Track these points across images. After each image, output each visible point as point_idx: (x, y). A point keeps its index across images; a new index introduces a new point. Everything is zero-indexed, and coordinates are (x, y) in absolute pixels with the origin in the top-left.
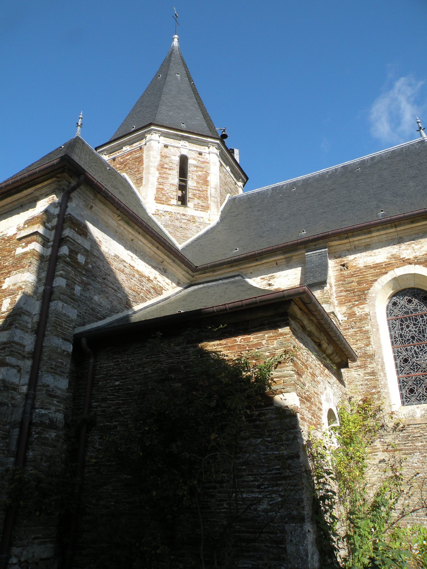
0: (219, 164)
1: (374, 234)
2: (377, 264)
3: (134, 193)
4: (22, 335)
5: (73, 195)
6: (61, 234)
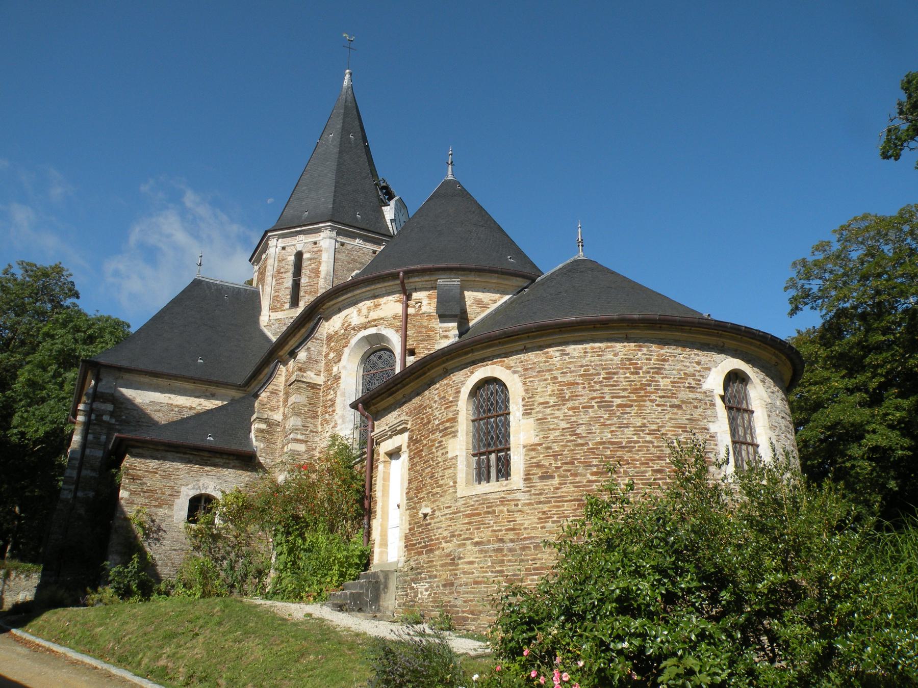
5: (101, 377)
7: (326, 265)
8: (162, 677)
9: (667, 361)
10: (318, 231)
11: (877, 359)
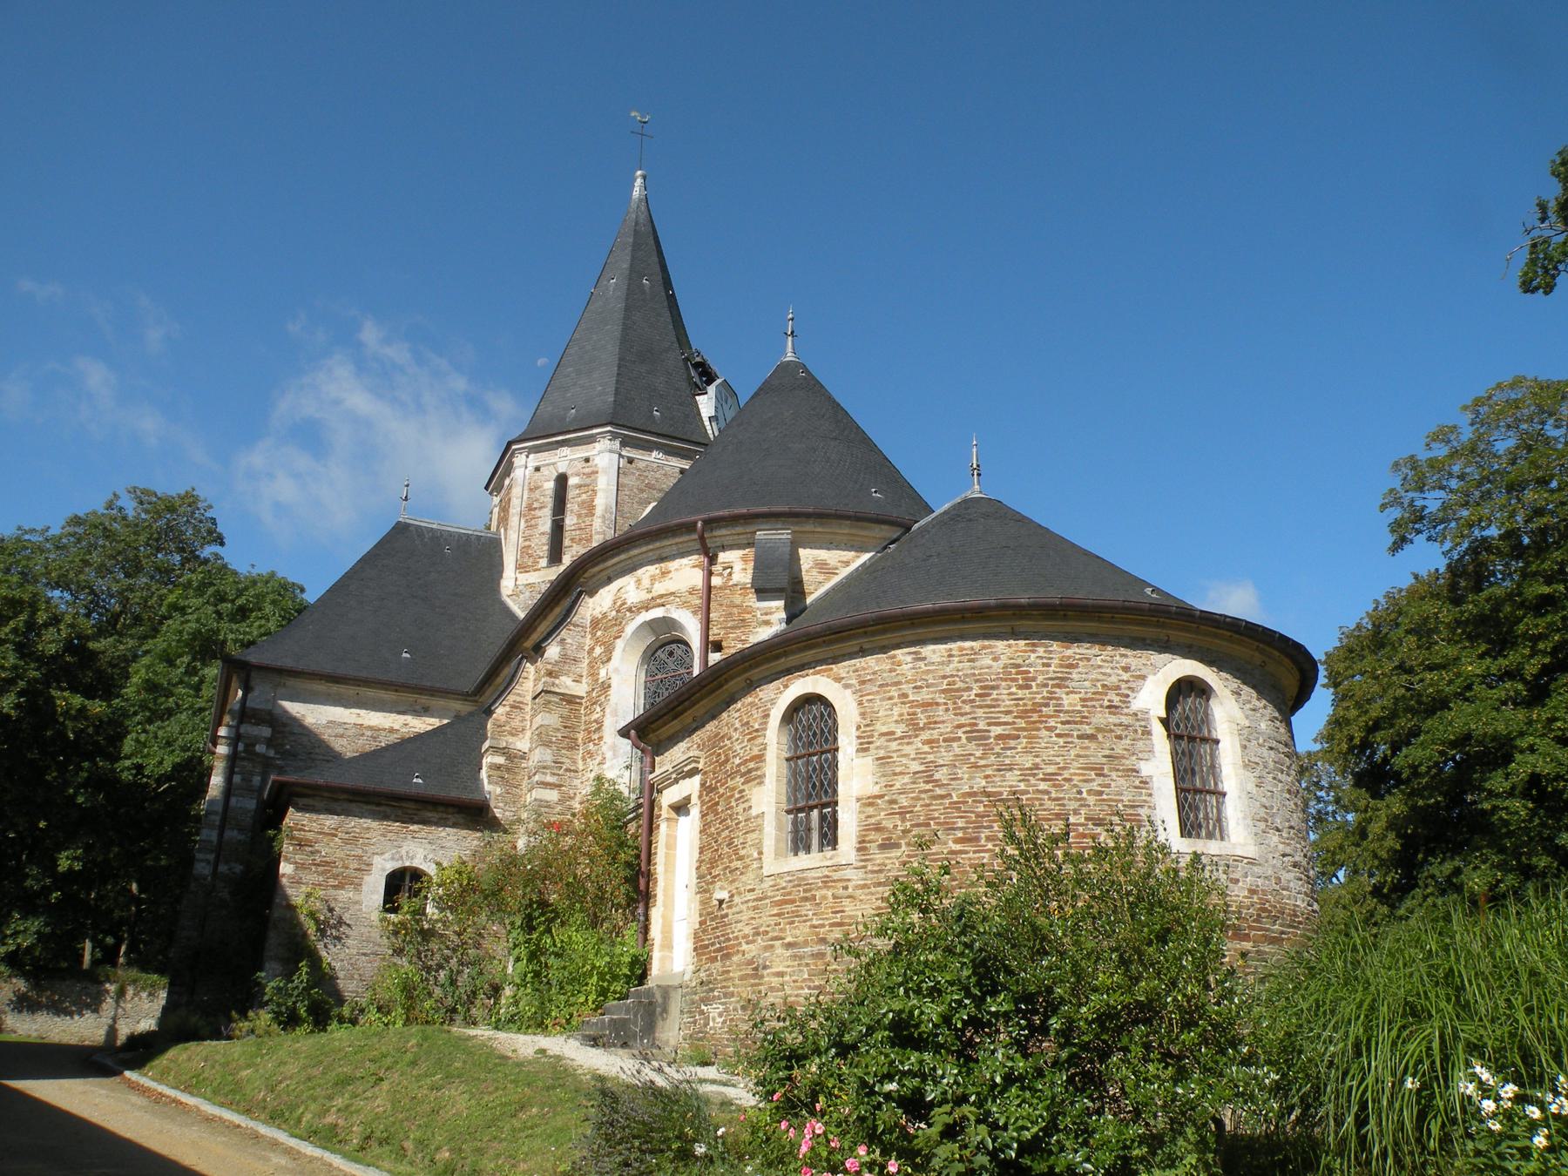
5: (252, 683)
7: (604, 498)
8: (330, 1140)
9: (1077, 666)
10: (591, 440)
11: (1537, 626)
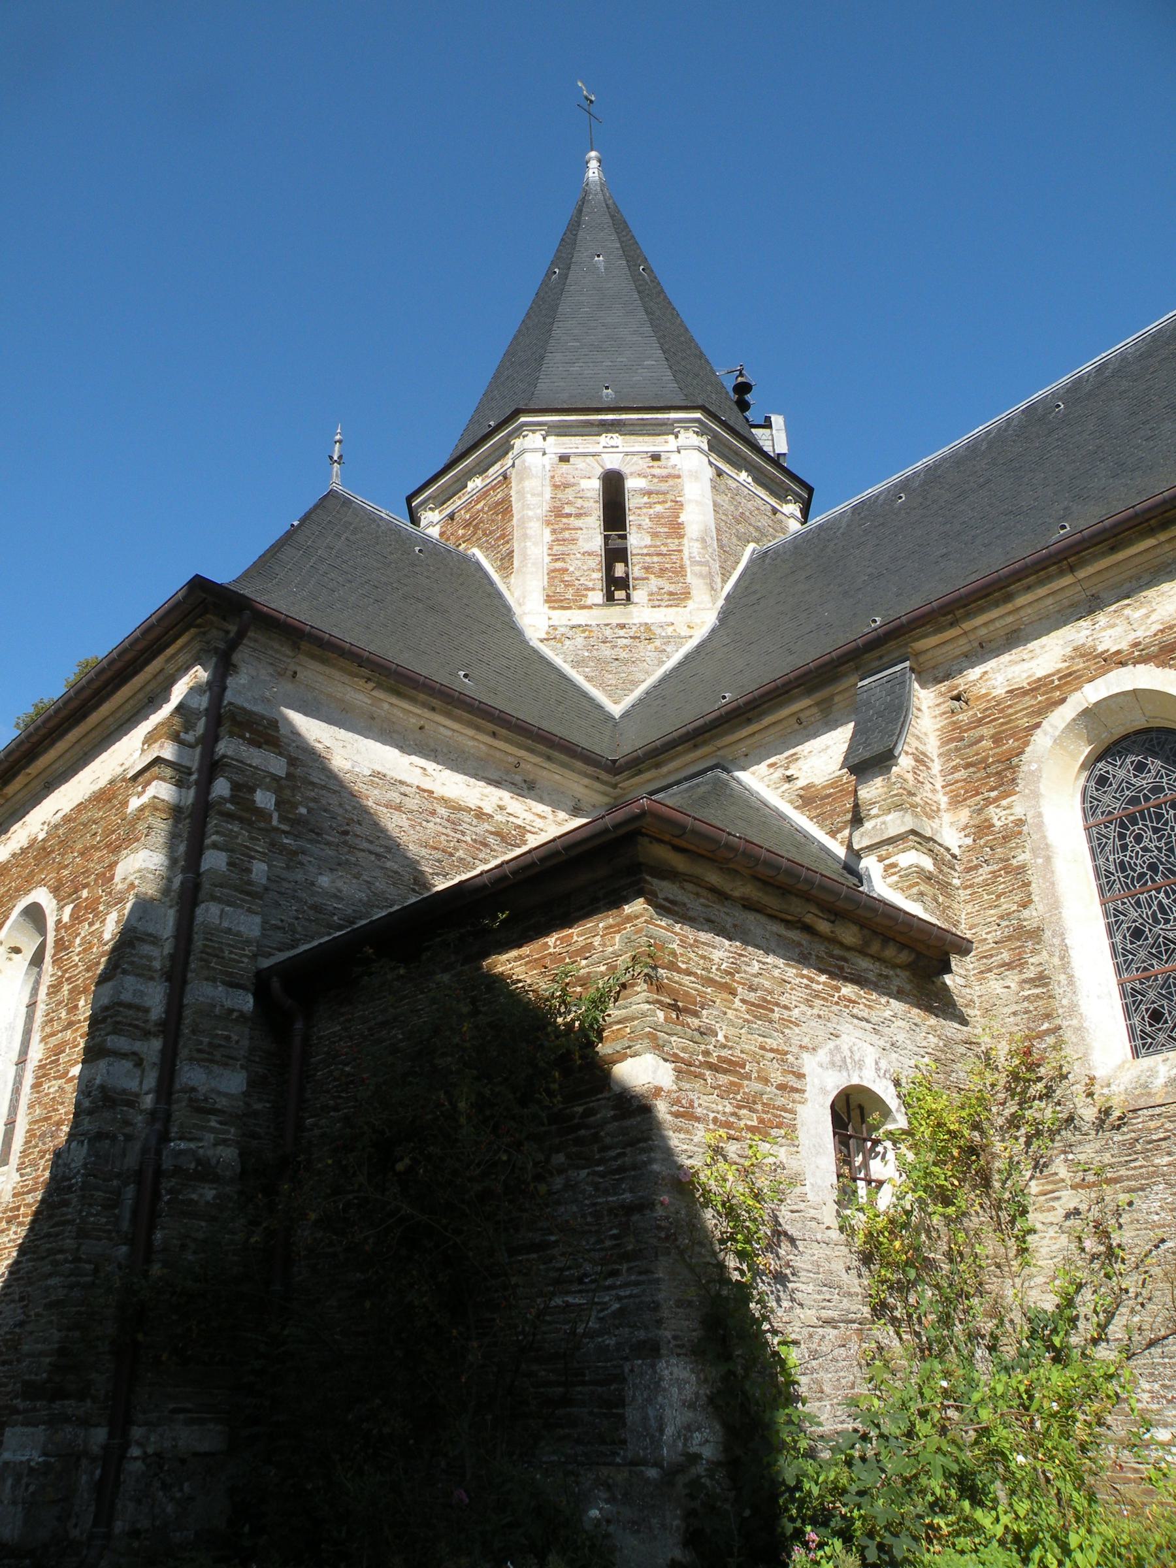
0: (710, 472)
1: (1020, 601)
2: (1040, 679)
3: (500, 595)
4: (139, 987)
5: (236, 657)
6: (213, 752)
